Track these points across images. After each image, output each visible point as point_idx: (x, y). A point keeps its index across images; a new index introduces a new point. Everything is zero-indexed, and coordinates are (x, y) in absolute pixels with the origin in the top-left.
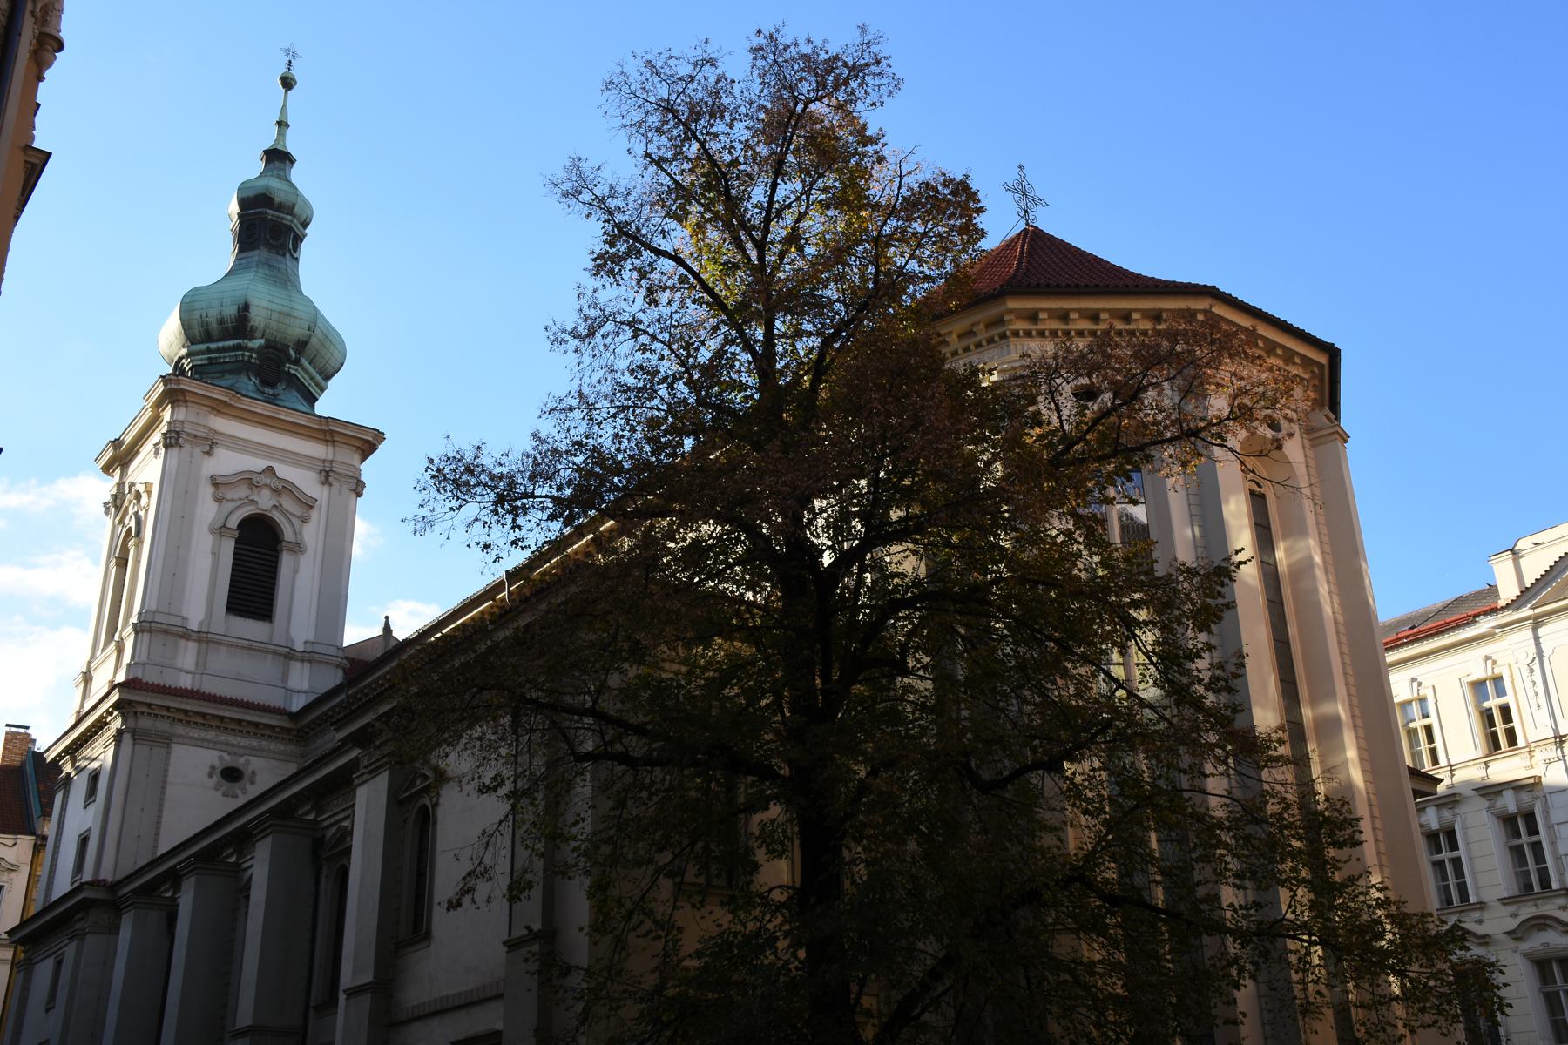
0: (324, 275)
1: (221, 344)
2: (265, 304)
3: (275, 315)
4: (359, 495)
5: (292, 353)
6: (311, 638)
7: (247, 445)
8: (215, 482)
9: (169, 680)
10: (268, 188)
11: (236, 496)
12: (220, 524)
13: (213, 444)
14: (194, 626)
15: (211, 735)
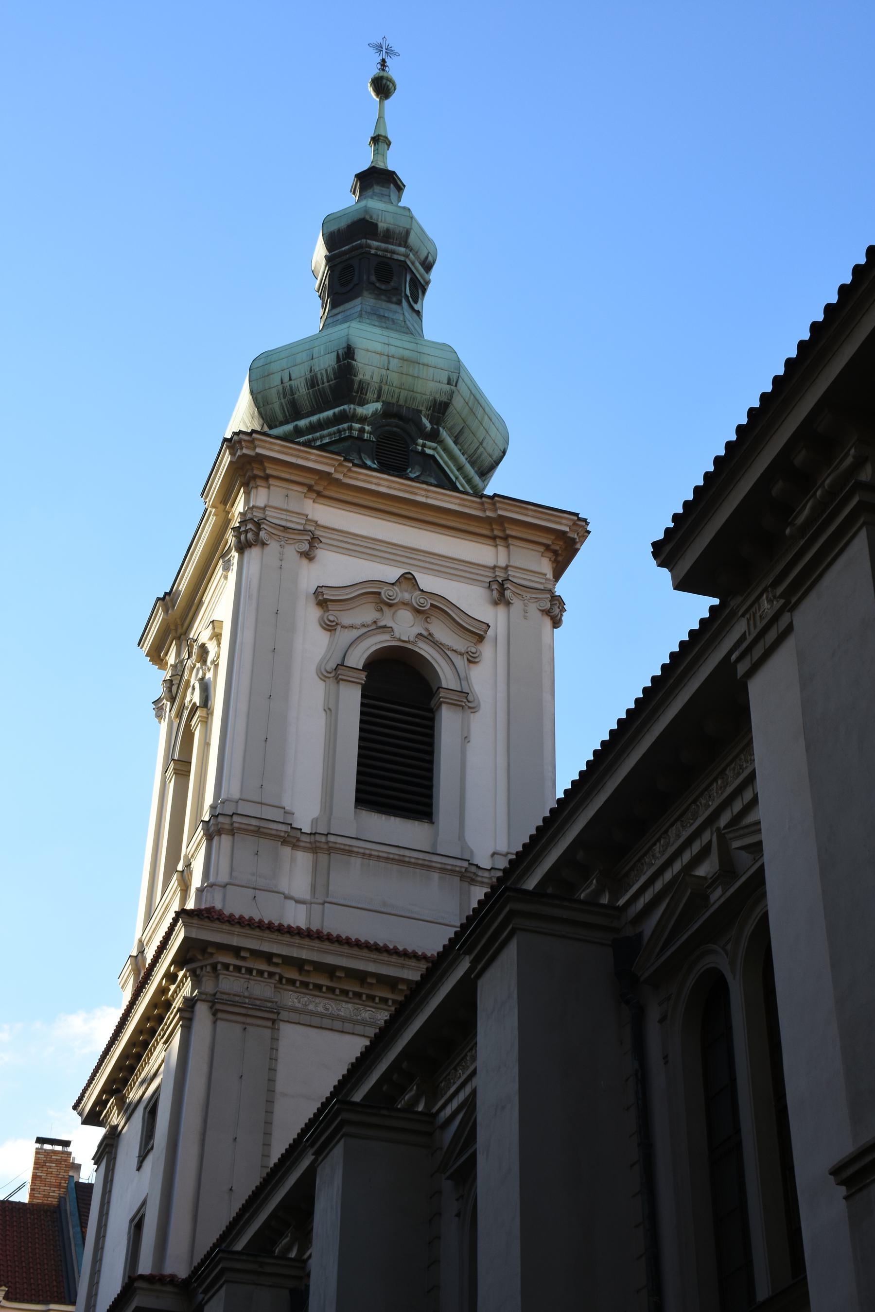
0: (464, 323)
2: (379, 347)
3: (394, 363)
4: (556, 623)
5: (425, 421)
7: (365, 543)
8: (323, 599)
9: (268, 912)
10: (366, 210)
11: (358, 621)
12: (332, 665)
13: (314, 541)
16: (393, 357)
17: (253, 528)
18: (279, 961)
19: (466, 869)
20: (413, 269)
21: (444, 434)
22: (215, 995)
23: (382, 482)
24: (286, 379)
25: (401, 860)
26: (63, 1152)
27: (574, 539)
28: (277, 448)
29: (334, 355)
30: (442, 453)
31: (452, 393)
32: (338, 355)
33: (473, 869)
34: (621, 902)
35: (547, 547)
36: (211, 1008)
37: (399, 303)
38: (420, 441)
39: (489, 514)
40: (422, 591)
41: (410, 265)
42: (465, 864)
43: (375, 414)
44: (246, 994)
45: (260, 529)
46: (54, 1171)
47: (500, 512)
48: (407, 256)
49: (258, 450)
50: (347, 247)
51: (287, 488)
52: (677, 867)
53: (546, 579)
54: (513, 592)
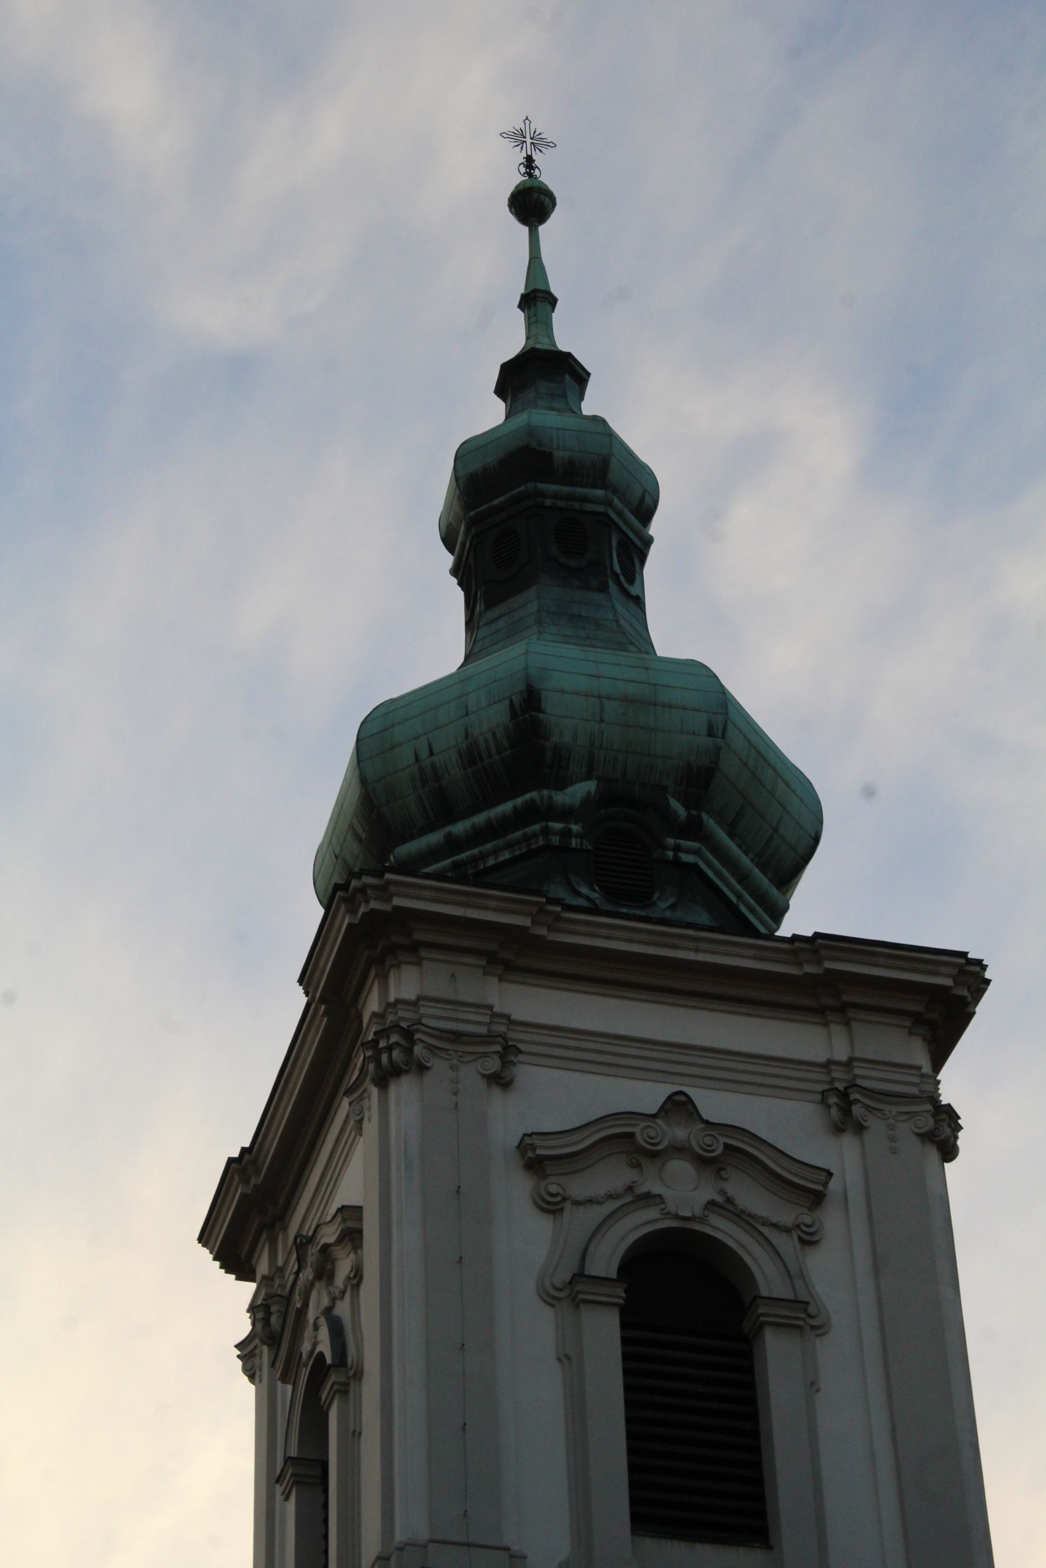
1: (480, 819)
4: (949, 1152)
5: (675, 805)
7: (592, 1056)
12: (563, 1276)
13: (509, 1052)
17: (402, 1042)
21: (710, 822)
24: (424, 753)
27: (963, 998)
28: (428, 894)
29: (507, 703)
30: (710, 856)
31: (718, 749)
37: (604, 588)
38: (671, 841)
40: (707, 1122)
45: (412, 1042)
47: (828, 965)
49: (397, 901)
50: (502, 499)
51: (450, 962)
53: (923, 1076)
54: (867, 1107)
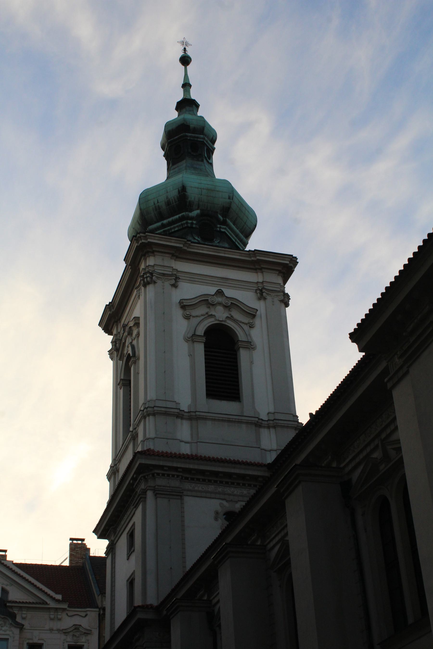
1: (170, 219)
4: (287, 305)
5: (220, 217)
6: (272, 410)
7: (198, 280)
9: (173, 449)
10: (184, 119)
12: (190, 335)
13: (177, 279)
14: (184, 407)
15: (211, 488)
16: (203, 189)
18: (181, 470)
19: (257, 421)
20: (207, 144)
21: (228, 221)
22: (155, 486)
23: (204, 249)
24: (156, 202)
25: (229, 420)
26: (82, 544)
27: (291, 267)
28: (157, 238)
29: (177, 190)
30: (228, 230)
31: (231, 202)
32: (179, 190)
33: (260, 421)
34: (342, 465)
35: (280, 272)
36: (154, 492)
37: (202, 161)
38: (219, 226)
39: (253, 259)
40: (227, 297)
41: (206, 143)
42: (257, 419)
43: (197, 215)
44: (168, 485)
45: (152, 276)
46: (79, 552)
48: (204, 139)
49: (149, 240)
52: (365, 453)
53: (281, 286)
54: (266, 293)
